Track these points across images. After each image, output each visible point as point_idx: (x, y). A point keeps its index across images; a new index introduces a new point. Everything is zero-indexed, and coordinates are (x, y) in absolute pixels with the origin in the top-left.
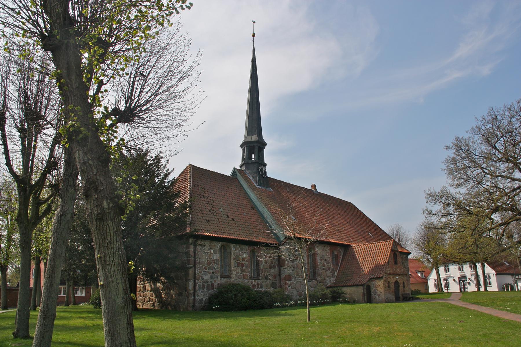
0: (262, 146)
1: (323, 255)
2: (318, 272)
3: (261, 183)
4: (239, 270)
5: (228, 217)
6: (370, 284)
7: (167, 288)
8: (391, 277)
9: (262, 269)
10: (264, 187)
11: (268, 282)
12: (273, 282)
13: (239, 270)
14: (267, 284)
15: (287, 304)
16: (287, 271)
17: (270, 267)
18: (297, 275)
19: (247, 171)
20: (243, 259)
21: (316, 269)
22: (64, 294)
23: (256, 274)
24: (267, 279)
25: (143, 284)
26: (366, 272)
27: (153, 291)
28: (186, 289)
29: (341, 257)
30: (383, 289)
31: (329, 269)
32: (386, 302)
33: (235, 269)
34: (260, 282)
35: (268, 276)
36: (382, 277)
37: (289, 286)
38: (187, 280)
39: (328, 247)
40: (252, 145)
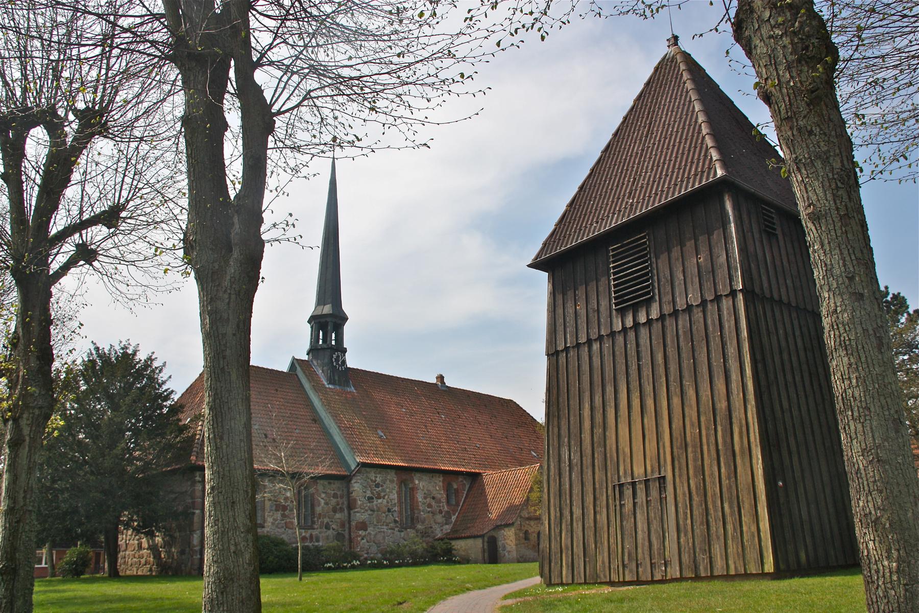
0: (339, 322)
1: (429, 491)
2: (418, 517)
3: (335, 381)
4: (278, 515)
5: (266, 436)
6: (496, 536)
7: (167, 544)
8: (532, 523)
9: (320, 514)
10: (340, 385)
11: (330, 532)
12: (338, 534)
13: (278, 515)
14: (328, 536)
15: (345, 565)
16: (360, 516)
17: (335, 510)
18: (379, 521)
19: (315, 362)
20: (286, 499)
21: (414, 513)
22: (46, 564)
23: (310, 521)
24: (327, 527)
25: (138, 540)
26: (493, 516)
27: (151, 549)
28: (189, 543)
29: (465, 492)
30: (514, 541)
31: (441, 512)
32: (519, 562)
33: (271, 514)
34: (315, 533)
35: (330, 523)
36: (513, 524)
37: (363, 539)
38: (192, 531)
39: (439, 477)
40: (323, 320)
